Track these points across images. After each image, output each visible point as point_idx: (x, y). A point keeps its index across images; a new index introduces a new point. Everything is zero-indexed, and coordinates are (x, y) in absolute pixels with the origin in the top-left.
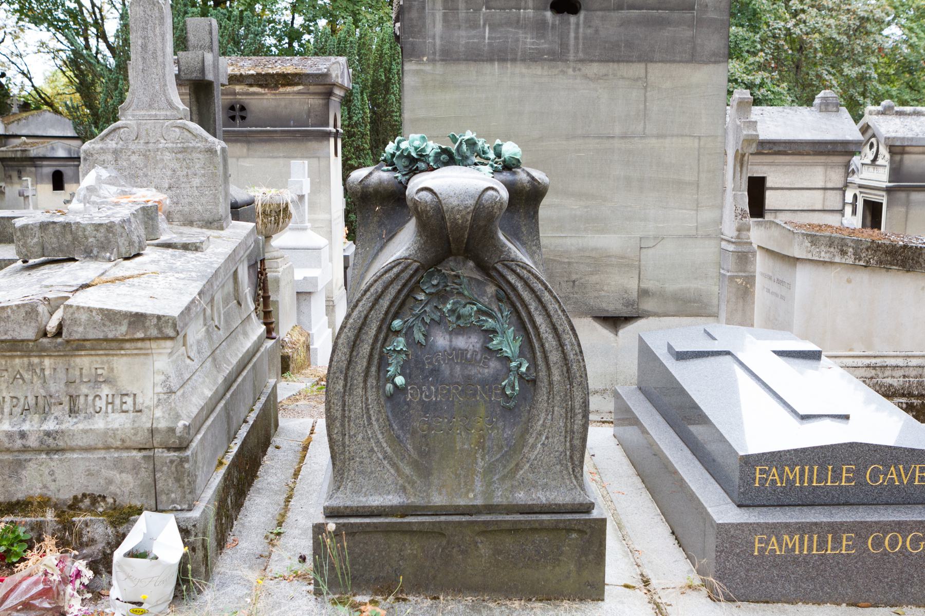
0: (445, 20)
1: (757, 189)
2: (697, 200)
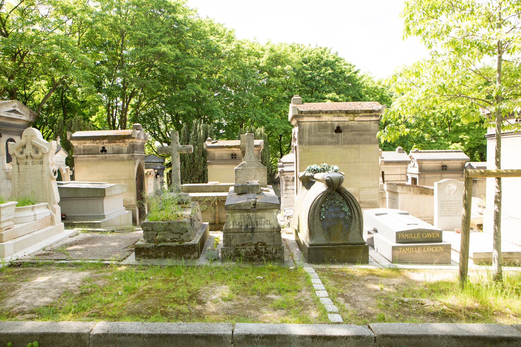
0: (309, 135)
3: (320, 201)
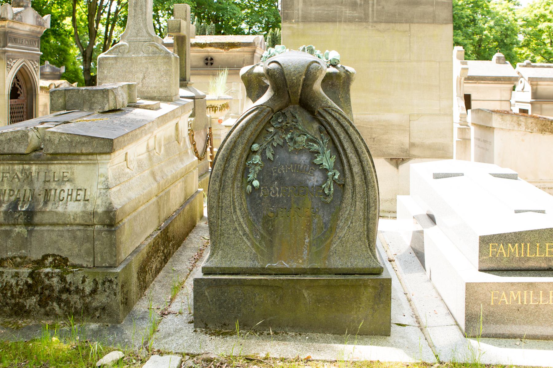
1: (468, 99)
3: (248, 133)
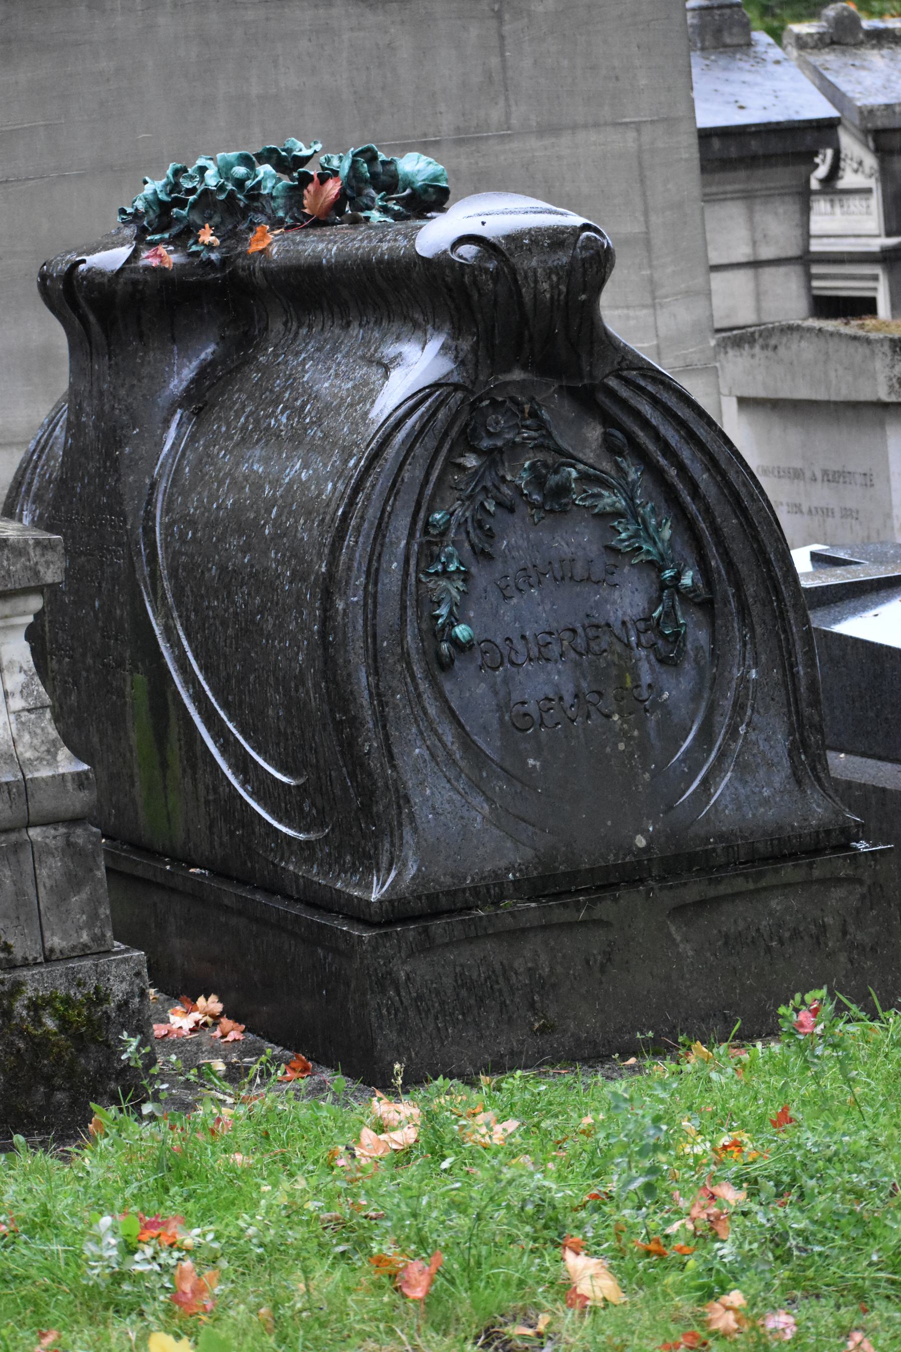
2: (651, 281)
